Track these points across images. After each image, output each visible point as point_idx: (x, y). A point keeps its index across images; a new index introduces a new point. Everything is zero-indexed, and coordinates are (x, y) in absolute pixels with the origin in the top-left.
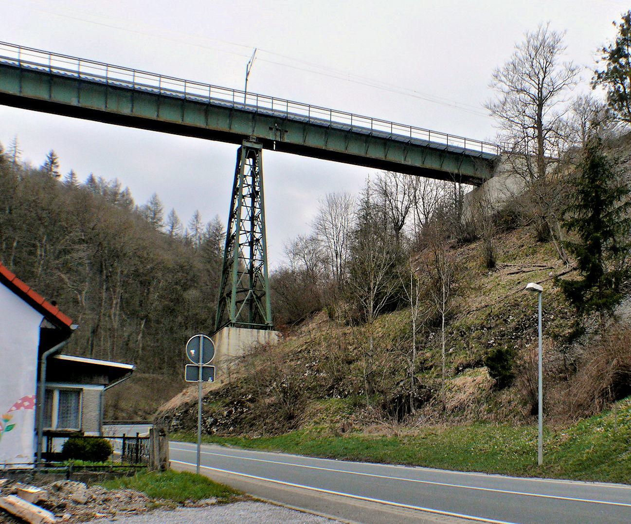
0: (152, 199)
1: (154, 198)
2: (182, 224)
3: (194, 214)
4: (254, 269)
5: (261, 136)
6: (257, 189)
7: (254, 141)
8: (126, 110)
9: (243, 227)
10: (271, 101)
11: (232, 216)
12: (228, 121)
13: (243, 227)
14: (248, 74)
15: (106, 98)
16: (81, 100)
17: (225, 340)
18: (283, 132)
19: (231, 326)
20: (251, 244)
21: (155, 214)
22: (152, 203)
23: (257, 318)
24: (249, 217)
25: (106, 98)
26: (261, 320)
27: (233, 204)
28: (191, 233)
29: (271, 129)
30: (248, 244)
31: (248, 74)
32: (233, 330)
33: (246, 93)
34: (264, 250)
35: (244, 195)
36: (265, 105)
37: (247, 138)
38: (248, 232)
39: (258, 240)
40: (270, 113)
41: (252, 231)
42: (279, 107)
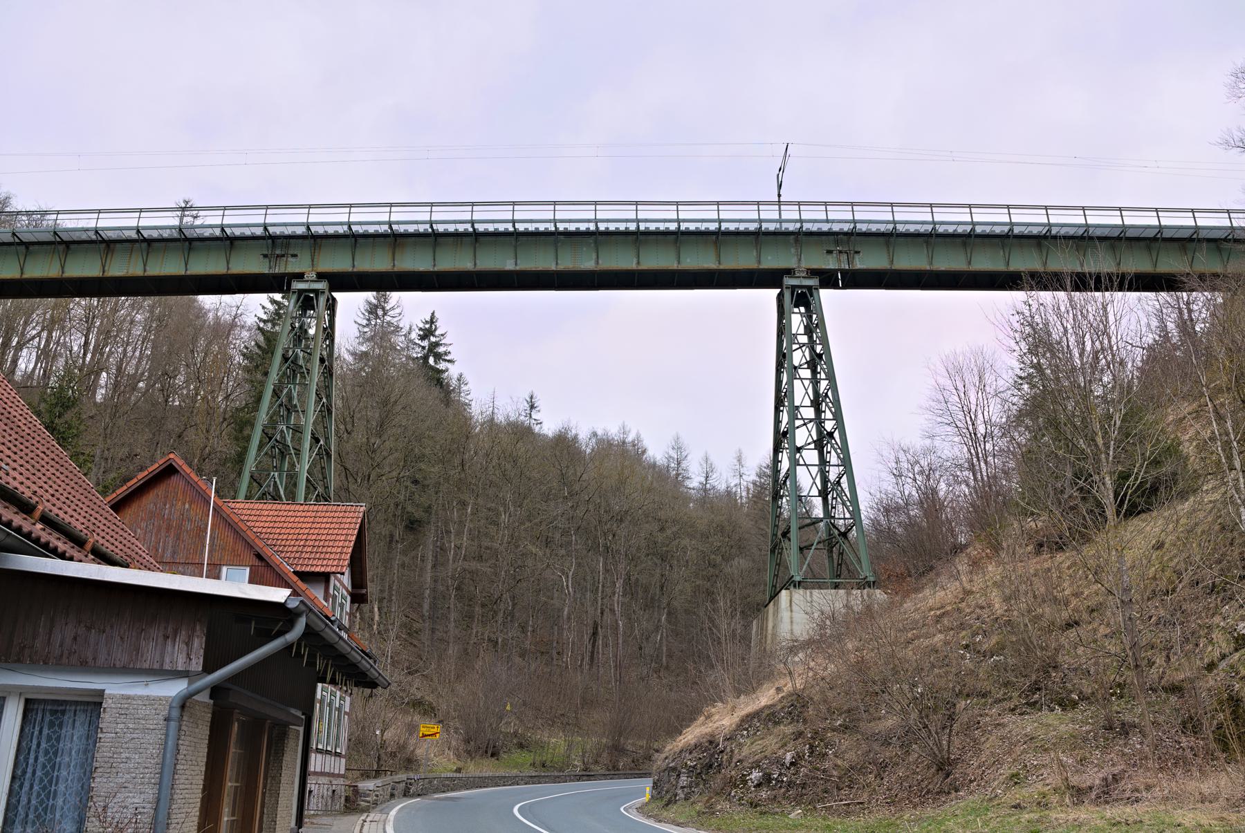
0: (673, 443)
1: (676, 442)
2: (721, 474)
3: (735, 455)
4: (829, 485)
5: (815, 266)
6: (819, 349)
7: (803, 275)
8: (587, 262)
9: (801, 459)
10: (823, 208)
11: (779, 403)
12: (755, 254)
13: (801, 459)
14: (780, 186)
15: (516, 247)
16: (518, 262)
17: (785, 615)
18: (851, 254)
19: (795, 586)
20: (819, 445)
21: (679, 463)
22: (673, 448)
23: (845, 572)
24: (809, 401)
25: (516, 247)
26: (852, 574)
27: (779, 382)
28: (734, 482)
29: (829, 252)
30: (812, 446)
31: (780, 186)
32: (799, 595)
33: (779, 203)
34: (844, 449)
35: (799, 446)
36: (813, 217)
37: (789, 272)
38: (811, 420)
39: (831, 435)
40: (825, 227)
41: (819, 421)
42: (840, 217)
